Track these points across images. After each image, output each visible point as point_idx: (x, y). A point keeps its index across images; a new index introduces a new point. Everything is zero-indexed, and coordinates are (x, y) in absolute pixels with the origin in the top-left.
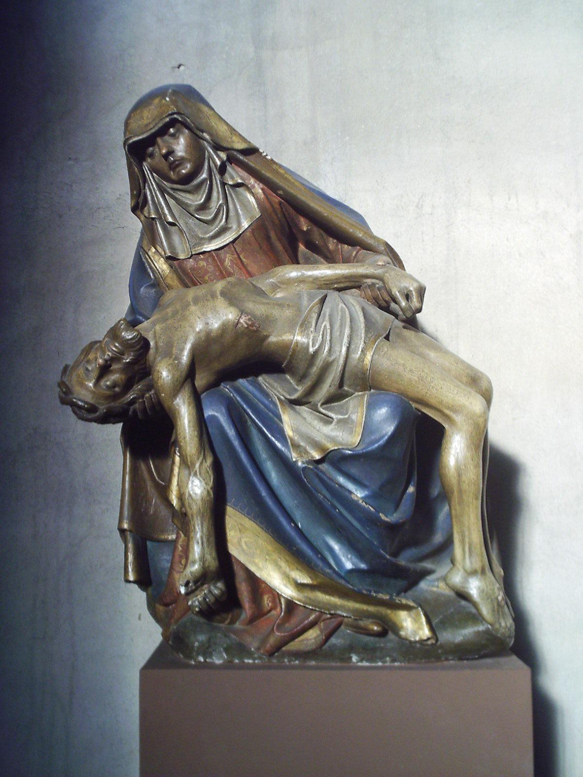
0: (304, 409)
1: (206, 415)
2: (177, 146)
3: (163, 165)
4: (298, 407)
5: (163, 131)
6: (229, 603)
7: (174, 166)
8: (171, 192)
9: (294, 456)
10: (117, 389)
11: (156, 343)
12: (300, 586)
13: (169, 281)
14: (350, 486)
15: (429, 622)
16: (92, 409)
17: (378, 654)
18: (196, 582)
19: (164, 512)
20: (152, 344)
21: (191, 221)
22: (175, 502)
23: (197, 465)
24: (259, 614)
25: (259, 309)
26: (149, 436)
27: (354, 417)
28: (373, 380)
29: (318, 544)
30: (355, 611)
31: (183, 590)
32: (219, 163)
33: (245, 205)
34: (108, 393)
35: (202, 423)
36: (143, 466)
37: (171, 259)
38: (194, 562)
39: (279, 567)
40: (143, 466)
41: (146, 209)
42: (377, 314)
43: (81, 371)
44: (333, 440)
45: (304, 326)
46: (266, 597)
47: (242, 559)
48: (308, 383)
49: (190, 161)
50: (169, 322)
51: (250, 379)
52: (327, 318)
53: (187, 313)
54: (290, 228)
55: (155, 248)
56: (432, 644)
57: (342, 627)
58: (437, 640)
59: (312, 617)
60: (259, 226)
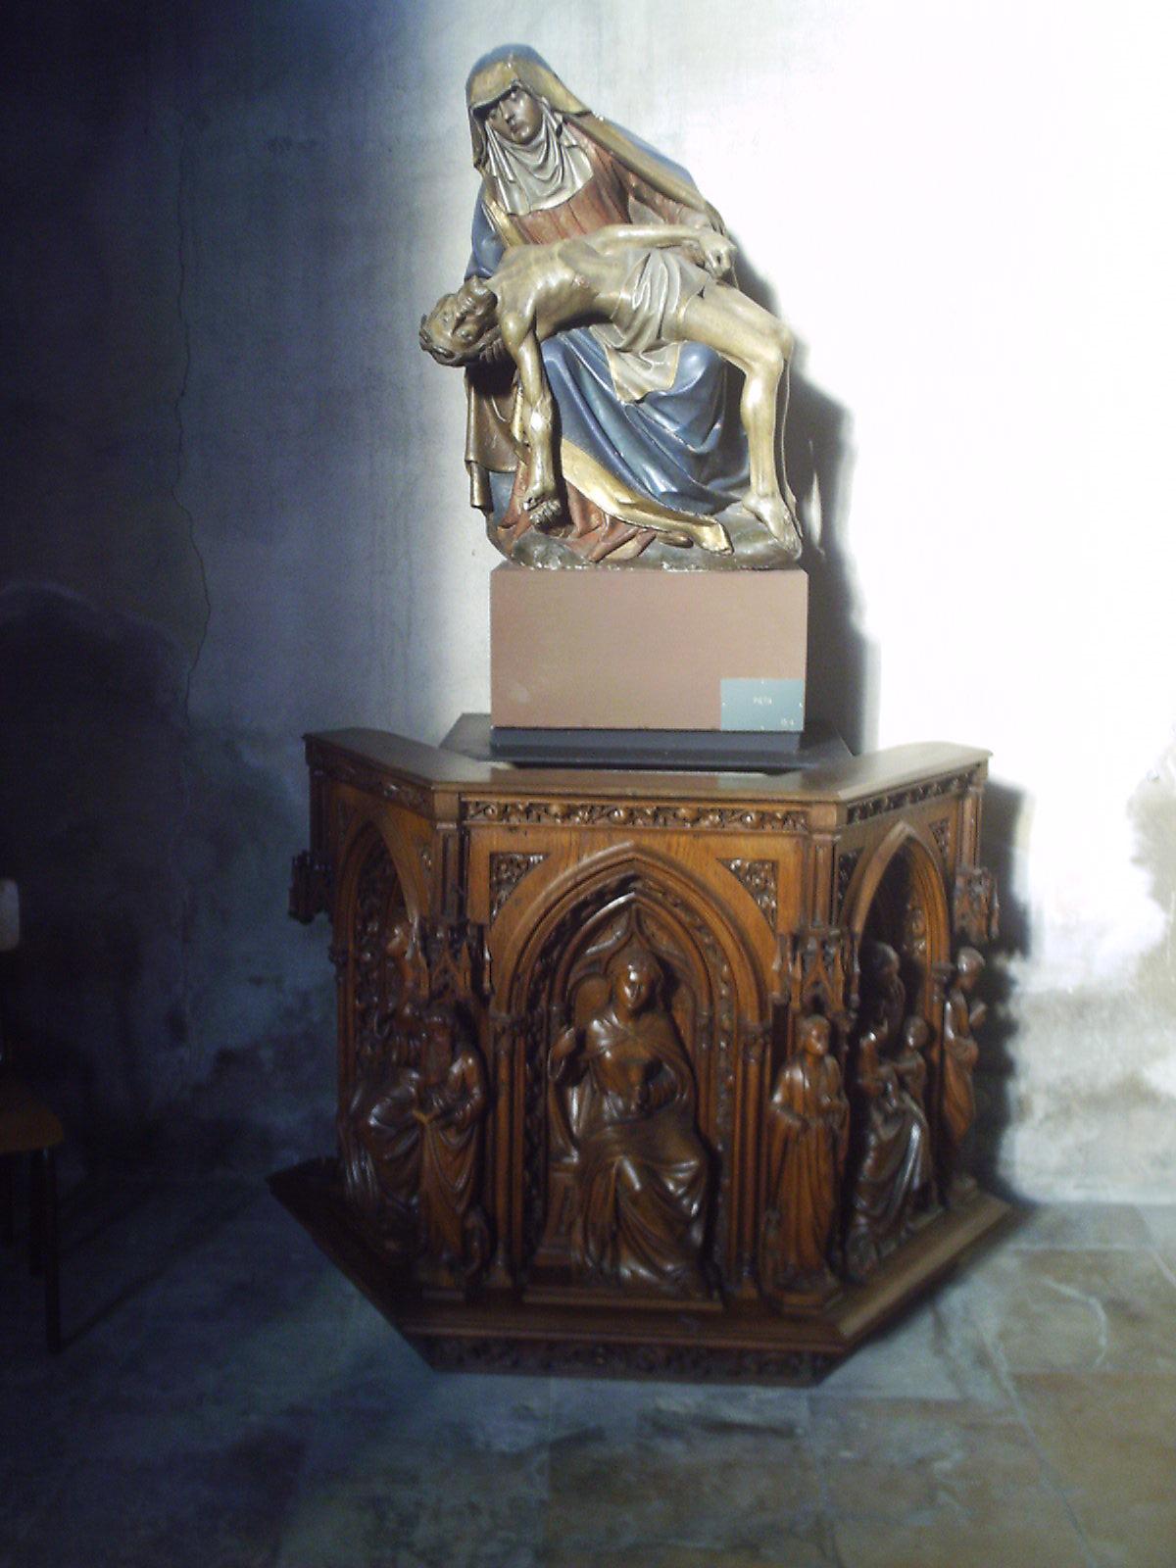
0: (627, 356)
1: (545, 361)
2: (518, 109)
3: (506, 128)
4: (622, 354)
5: (505, 96)
6: (563, 519)
7: (515, 129)
8: (512, 151)
9: (618, 397)
10: (470, 338)
11: (503, 298)
12: (623, 505)
13: (510, 235)
14: (665, 422)
15: (727, 536)
16: (450, 355)
17: (685, 562)
18: (536, 500)
19: (505, 446)
20: (499, 298)
21: (531, 180)
22: (517, 434)
23: (538, 403)
24: (588, 530)
25: (590, 268)
26: (492, 377)
27: (669, 364)
28: (686, 332)
29: (638, 471)
30: (666, 526)
31: (526, 506)
32: (556, 126)
33: (579, 166)
34: (463, 341)
35: (542, 368)
36: (486, 405)
37: (511, 215)
38: (535, 483)
39: (604, 489)
40: (486, 405)
41: (487, 165)
42: (695, 273)
43: (438, 321)
44: (651, 383)
45: (629, 285)
46: (593, 516)
47: (574, 484)
48: (632, 333)
49: (528, 125)
50: (515, 279)
51: (582, 328)
52: (648, 279)
53: (529, 272)
54: (620, 182)
55: (497, 202)
56: (729, 554)
57: (656, 540)
58: (733, 551)
59: (631, 531)
60: (593, 187)
